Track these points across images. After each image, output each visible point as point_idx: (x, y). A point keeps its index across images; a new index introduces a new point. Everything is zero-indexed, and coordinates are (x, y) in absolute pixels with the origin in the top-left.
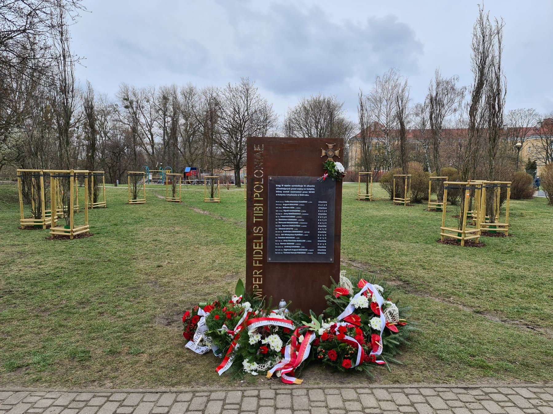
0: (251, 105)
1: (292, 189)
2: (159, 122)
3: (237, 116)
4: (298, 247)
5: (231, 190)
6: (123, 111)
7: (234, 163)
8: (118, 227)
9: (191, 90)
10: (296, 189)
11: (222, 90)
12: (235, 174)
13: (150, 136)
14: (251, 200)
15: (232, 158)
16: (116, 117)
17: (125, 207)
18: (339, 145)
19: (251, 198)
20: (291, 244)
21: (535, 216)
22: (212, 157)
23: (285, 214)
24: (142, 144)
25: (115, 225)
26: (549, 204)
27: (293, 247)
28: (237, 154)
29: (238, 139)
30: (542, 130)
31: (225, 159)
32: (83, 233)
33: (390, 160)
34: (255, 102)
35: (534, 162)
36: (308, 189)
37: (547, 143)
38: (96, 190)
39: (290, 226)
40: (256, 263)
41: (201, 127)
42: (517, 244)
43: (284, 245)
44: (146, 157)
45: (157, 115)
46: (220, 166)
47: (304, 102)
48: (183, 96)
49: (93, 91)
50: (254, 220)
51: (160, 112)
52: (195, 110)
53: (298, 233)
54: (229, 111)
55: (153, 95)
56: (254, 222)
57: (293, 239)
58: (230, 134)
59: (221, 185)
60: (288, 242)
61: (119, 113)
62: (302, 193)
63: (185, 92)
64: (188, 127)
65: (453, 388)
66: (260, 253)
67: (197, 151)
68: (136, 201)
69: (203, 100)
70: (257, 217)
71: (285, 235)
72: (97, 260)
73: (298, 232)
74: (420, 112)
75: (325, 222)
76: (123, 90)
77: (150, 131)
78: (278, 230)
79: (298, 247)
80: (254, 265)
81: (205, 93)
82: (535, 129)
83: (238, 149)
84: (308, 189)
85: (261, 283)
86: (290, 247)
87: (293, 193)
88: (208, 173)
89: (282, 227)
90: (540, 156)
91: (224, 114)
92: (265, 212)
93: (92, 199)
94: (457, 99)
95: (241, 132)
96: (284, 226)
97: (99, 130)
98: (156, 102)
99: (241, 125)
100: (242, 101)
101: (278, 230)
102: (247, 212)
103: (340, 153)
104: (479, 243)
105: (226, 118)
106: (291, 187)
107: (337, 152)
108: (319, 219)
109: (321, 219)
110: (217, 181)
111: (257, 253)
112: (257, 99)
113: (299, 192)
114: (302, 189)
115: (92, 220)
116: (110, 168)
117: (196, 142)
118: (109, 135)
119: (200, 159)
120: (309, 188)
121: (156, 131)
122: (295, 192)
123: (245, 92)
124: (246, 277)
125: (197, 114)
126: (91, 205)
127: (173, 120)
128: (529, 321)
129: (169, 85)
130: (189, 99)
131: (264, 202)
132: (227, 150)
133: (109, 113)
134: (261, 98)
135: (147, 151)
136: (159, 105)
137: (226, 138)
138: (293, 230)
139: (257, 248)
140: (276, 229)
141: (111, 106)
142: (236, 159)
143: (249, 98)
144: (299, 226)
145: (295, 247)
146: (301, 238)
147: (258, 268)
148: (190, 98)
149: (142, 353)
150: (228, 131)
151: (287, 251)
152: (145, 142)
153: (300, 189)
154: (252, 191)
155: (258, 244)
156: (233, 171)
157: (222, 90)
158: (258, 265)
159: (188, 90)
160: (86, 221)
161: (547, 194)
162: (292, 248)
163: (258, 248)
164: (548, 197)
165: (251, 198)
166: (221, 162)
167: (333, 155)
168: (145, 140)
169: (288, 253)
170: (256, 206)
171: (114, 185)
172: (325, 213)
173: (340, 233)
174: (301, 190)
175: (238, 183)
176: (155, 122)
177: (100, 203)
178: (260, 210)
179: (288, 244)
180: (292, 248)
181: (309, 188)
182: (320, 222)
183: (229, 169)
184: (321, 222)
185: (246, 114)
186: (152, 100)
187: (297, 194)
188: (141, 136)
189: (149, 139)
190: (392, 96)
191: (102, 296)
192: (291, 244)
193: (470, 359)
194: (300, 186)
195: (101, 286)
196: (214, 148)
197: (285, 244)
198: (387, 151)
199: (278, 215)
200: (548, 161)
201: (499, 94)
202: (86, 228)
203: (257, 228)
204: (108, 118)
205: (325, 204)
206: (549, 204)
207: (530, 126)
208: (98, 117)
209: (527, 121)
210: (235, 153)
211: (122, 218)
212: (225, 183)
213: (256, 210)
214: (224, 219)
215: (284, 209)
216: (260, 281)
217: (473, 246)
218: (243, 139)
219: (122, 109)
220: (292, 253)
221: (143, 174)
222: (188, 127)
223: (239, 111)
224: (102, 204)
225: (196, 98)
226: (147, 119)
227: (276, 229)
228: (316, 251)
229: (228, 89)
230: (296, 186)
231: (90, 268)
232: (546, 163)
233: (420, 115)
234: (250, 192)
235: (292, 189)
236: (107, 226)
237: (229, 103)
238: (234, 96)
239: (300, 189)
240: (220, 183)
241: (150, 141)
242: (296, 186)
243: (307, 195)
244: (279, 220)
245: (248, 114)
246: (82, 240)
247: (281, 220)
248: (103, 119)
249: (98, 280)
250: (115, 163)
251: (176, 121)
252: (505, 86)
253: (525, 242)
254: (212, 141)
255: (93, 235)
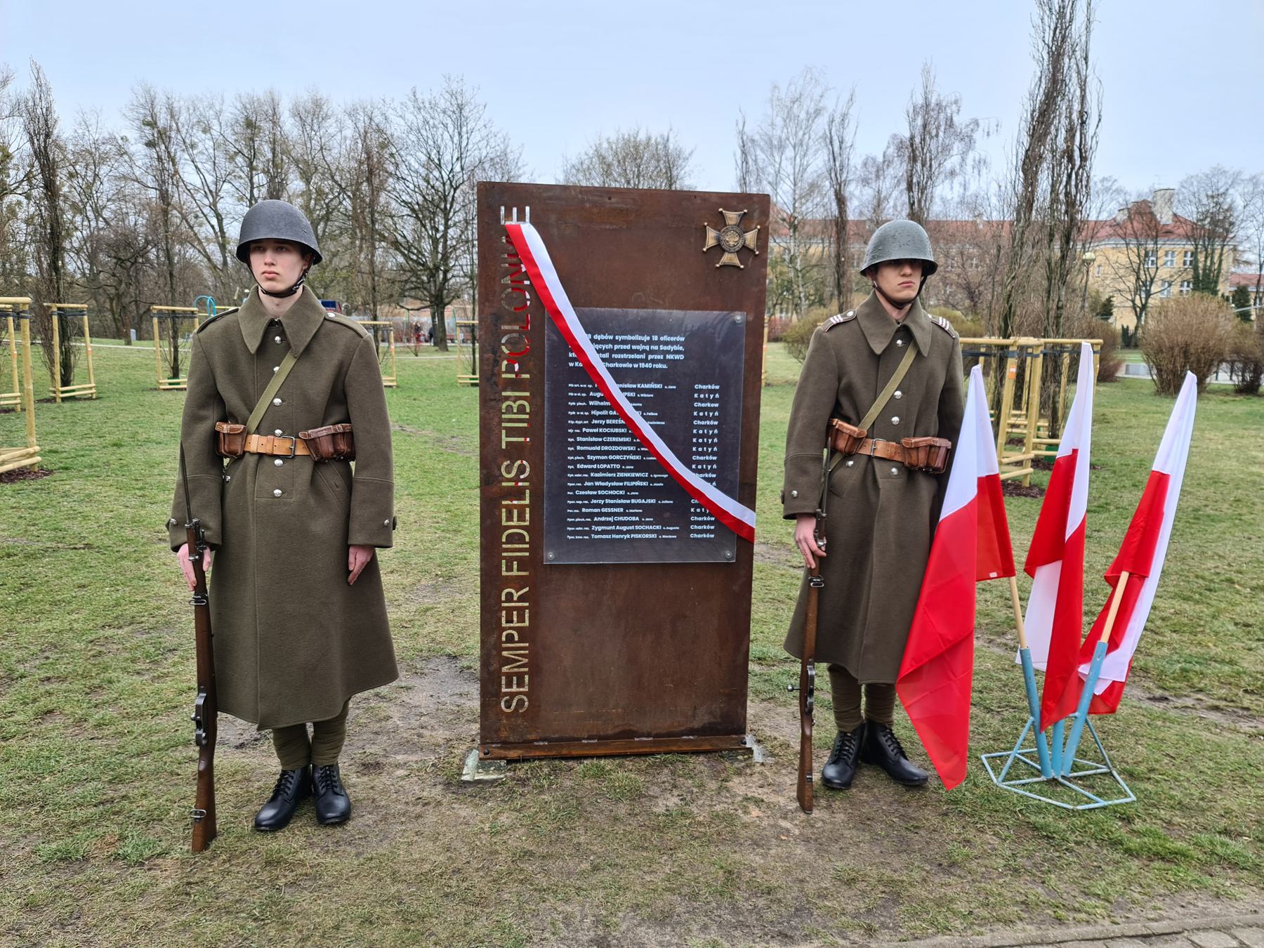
0: (470, 146)
1: (616, 347)
2: (237, 185)
3: (436, 173)
4: (634, 519)
5: (423, 357)
6: (143, 152)
7: (429, 292)
8: (122, 450)
9: (318, 104)
10: (628, 347)
11: (396, 104)
12: (433, 318)
13: (214, 221)
14: (494, 379)
15: (425, 278)
16: (124, 169)
17: (149, 397)
18: (756, 215)
19: (493, 374)
20: (613, 510)
21: (1134, 422)
22: (372, 272)
23: (595, 422)
24: (195, 240)
25: (115, 445)
26: (1158, 393)
27: (621, 519)
28: (437, 268)
29: (437, 230)
30: (1130, 226)
31: (406, 282)
32: (25, 467)
33: (801, 289)
34: (478, 138)
35: (1109, 300)
36: (665, 348)
37: (1139, 256)
38: (66, 354)
39: (611, 457)
40: (509, 568)
41: (344, 199)
42: (1115, 488)
43: (592, 515)
44: (207, 274)
45: (230, 167)
46: (395, 299)
47: (600, 144)
48: (298, 119)
49: (49, 89)
50: (505, 439)
51: (239, 159)
52: (328, 159)
53: (635, 479)
54: (415, 160)
55: (218, 115)
56: (504, 446)
57: (620, 497)
58: (417, 217)
59: (399, 344)
60: (606, 505)
61: (131, 160)
62: (646, 361)
63: (301, 109)
64: (313, 202)
65: (1112, 938)
66: (521, 539)
67: (336, 260)
68: (178, 384)
69: (349, 132)
70: (511, 432)
71: (597, 484)
72: (54, 544)
73: (633, 475)
74: (873, 176)
75: (713, 445)
76: (142, 101)
77: (213, 206)
78: (576, 471)
79: (634, 519)
80: (504, 573)
81: (352, 114)
82: (1115, 225)
83: (440, 256)
84: (665, 348)
85: (527, 624)
86: (611, 519)
87: (619, 361)
88: (365, 314)
89: (586, 462)
90: (1122, 286)
91: (403, 168)
92: (536, 414)
93: (58, 377)
94: (957, 147)
95: (446, 213)
96: (594, 458)
97: (81, 201)
98: (228, 133)
99: (444, 198)
100: (446, 136)
101: (576, 471)
102: (482, 418)
103: (758, 238)
104: (1032, 486)
105: (409, 178)
106: (614, 342)
107: (751, 238)
108: (695, 436)
109: (702, 436)
110: (388, 334)
111: (512, 539)
112: (484, 132)
113: (638, 357)
114: (647, 348)
115: (55, 432)
116: (111, 300)
117: (333, 238)
118: (106, 214)
119: (345, 279)
120: (666, 343)
121: (229, 208)
122: (625, 356)
123: (454, 112)
124: (482, 608)
125: (333, 168)
126: (54, 392)
127: (272, 179)
128: (1220, 699)
129: (260, 92)
130: (312, 129)
131: (534, 386)
132: (412, 259)
133: (104, 159)
134: (494, 130)
135: (209, 259)
136: (236, 140)
137: (407, 228)
138: (621, 470)
139: (514, 524)
140: (570, 467)
141: (111, 139)
142: (435, 281)
143: (464, 129)
144: (638, 457)
145: (626, 519)
146: (644, 493)
147: (518, 583)
148: (316, 127)
149: (159, 855)
150: (413, 210)
151: (603, 532)
152: (203, 235)
153: (640, 347)
154: (494, 353)
155: (515, 512)
156: (428, 312)
157: (396, 104)
158: (515, 573)
159: (309, 106)
160: (31, 434)
161: (1155, 371)
162: (616, 523)
163: (515, 523)
164: (1155, 377)
165: (493, 374)
166: (397, 287)
167: (740, 245)
168: (203, 229)
169: (604, 537)
170: (507, 398)
171: (123, 341)
172: (714, 418)
173: (755, 476)
174: (644, 351)
175: (439, 337)
176: (226, 186)
177: (77, 388)
178: (521, 410)
179: (604, 510)
180: (616, 523)
181: (666, 343)
182: (698, 445)
183: (418, 304)
184: (702, 445)
185: (457, 168)
186: (216, 127)
187: (633, 361)
188: (192, 221)
189: (213, 227)
190: (807, 137)
191: (53, 656)
192: (613, 510)
193: (1118, 829)
194: (640, 338)
195: (57, 624)
196: (379, 252)
197: (596, 510)
198: (794, 268)
199: (576, 426)
200: (1138, 297)
201: (1083, 123)
202: (32, 455)
203: (513, 463)
204: (104, 170)
205: (714, 392)
206: (1158, 393)
207: (1103, 217)
208: (77, 167)
209: (1099, 205)
210: (431, 265)
211: (136, 428)
212: (409, 341)
213: (509, 409)
214: (408, 428)
215: (595, 408)
216: (521, 619)
217: (1018, 495)
218: (451, 231)
219: (138, 149)
220: (618, 537)
221: (193, 312)
222: (313, 202)
223: (439, 160)
224: (85, 389)
225: (331, 126)
226: (207, 176)
227: (570, 467)
228: (686, 529)
229: (410, 104)
230: (629, 338)
231: (31, 567)
232: (1133, 301)
233: (873, 185)
234: (490, 355)
235: (616, 347)
236: (91, 448)
237: (414, 138)
238: (426, 122)
239: (640, 347)
240: (396, 341)
241: (216, 233)
242: (629, 338)
243: (659, 366)
244: (579, 439)
245: (462, 169)
246: (17, 486)
247: (584, 439)
248: (90, 173)
249: (47, 607)
250: (123, 285)
251: (281, 183)
252: (1099, 103)
253: (1131, 483)
254: (373, 236)
255: (50, 472)
